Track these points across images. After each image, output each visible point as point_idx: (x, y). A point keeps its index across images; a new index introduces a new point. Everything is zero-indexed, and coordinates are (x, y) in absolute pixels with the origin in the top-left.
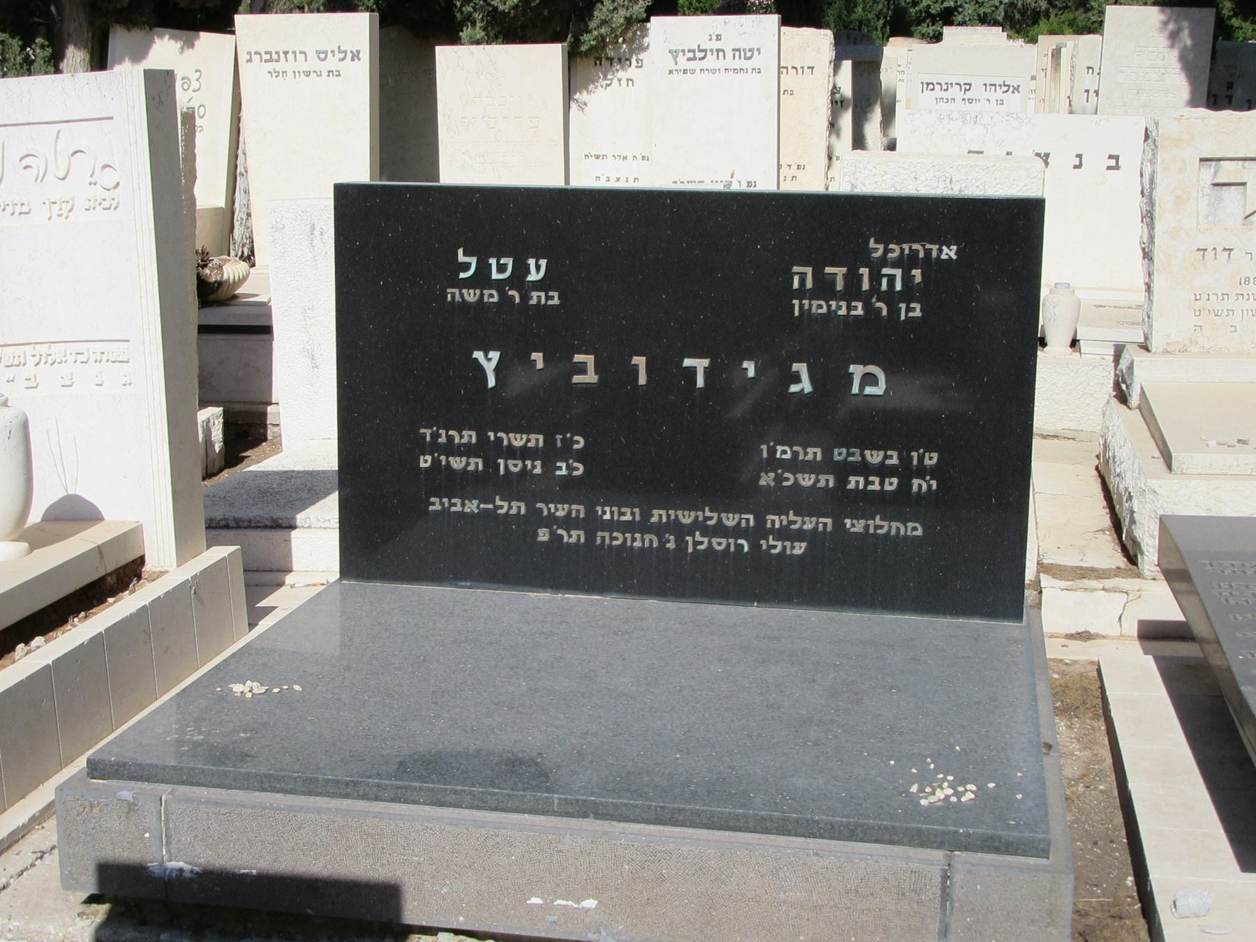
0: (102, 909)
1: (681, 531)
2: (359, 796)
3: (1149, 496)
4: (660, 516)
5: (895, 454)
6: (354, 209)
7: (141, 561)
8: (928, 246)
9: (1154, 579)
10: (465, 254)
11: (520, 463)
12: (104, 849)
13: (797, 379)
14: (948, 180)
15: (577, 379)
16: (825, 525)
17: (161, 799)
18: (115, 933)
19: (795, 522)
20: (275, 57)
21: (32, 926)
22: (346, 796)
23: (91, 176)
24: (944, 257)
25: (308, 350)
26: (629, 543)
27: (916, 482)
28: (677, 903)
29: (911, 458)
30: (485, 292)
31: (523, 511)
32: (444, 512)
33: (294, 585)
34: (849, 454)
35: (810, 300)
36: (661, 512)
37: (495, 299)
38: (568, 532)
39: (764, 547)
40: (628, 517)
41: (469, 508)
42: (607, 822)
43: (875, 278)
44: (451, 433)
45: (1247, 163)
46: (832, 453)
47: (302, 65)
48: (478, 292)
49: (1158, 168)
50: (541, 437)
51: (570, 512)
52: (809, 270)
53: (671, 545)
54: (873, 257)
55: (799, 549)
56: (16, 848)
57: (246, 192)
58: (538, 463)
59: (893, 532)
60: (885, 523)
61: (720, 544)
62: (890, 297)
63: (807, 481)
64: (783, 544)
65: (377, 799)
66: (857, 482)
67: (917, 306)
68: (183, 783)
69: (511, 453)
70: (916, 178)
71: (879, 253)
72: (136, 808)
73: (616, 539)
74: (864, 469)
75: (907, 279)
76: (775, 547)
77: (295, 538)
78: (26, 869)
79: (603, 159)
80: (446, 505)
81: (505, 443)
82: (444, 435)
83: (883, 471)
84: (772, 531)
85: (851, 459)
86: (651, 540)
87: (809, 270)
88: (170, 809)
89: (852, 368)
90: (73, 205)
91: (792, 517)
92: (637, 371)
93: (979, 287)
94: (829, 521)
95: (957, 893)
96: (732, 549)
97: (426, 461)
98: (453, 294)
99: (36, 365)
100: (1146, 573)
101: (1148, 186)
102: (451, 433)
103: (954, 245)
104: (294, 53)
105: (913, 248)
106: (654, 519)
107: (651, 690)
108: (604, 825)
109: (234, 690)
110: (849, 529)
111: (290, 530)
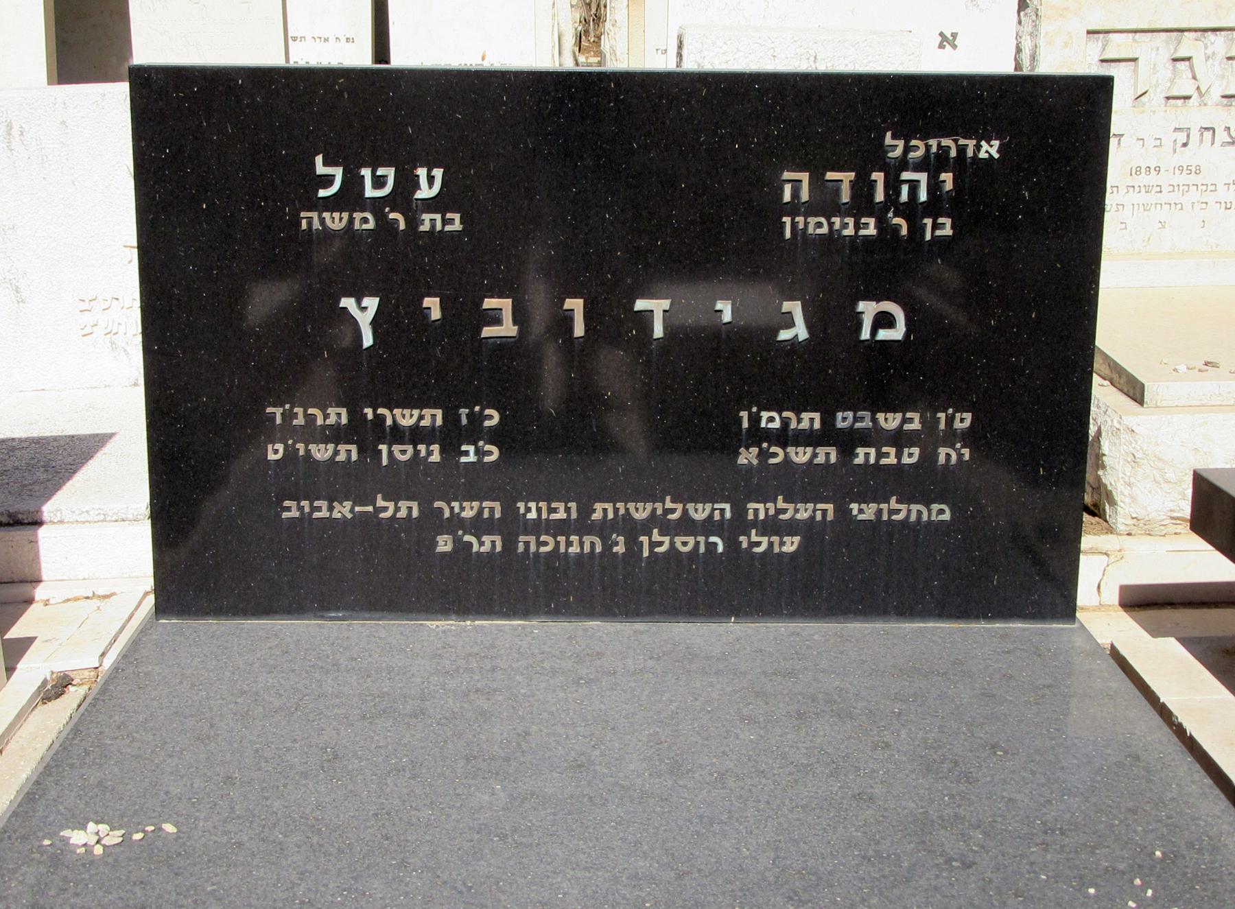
1: (632, 529)
3: (1125, 436)
4: (605, 510)
5: (916, 416)
6: (161, 103)
8: (962, 142)
9: (1129, 534)
10: (325, 164)
11: (410, 449)
14: (812, 58)
15: (487, 332)
16: (824, 512)
19: (785, 511)
25: (10, 280)
26: (562, 549)
27: (942, 451)
30: (355, 215)
31: (415, 513)
32: (304, 519)
33: (48, 600)
34: (856, 419)
35: (806, 216)
36: (606, 505)
37: (371, 225)
38: (479, 538)
39: (745, 545)
40: (561, 515)
41: (340, 512)
43: (893, 185)
44: (310, 411)
46: (834, 419)
48: (345, 215)
49: (1042, 42)
50: (439, 413)
51: (481, 511)
52: (804, 177)
53: (620, 549)
54: (889, 158)
55: (791, 545)
58: (436, 448)
59: (913, 517)
62: (912, 211)
63: (801, 455)
64: (769, 539)
66: (867, 455)
67: (947, 221)
69: (397, 435)
70: (774, 56)
71: (898, 152)
73: (546, 544)
75: (934, 186)
76: (758, 544)
77: (43, 538)
79: (301, 41)
80: (307, 510)
81: (389, 422)
82: (301, 415)
83: (899, 439)
84: (755, 523)
85: (858, 425)
86: (592, 543)
87: (804, 177)
89: (862, 306)
91: (781, 504)
92: (572, 319)
93: (1027, 195)
94: (830, 507)
96: (702, 549)
98: (310, 220)
100: (1121, 527)
101: (1028, 64)
102: (310, 411)
103: (996, 139)
105: (943, 144)
106: (597, 516)
107: (681, 783)
109: (72, 841)
110: (856, 516)
111: (37, 526)
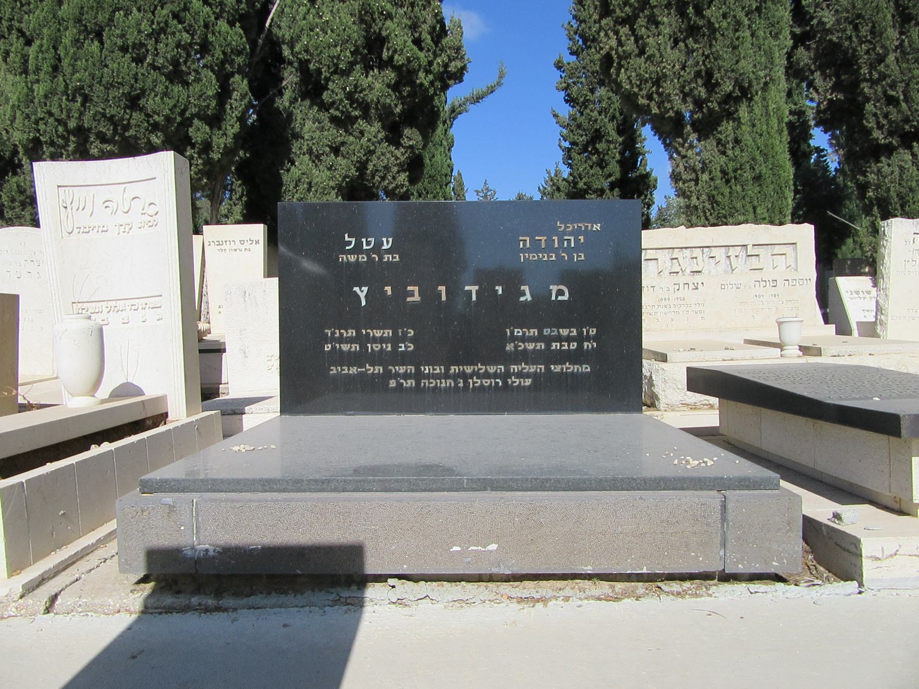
0: (149, 587)
1: (465, 377)
2: (331, 489)
4: (455, 369)
7: (167, 414)
12: (151, 540)
13: (524, 294)
17: (193, 501)
18: (158, 600)
20: (221, 243)
21: (97, 601)
22: (323, 490)
23: (143, 210)
24: (594, 229)
26: (439, 385)
27: (586, 344)
28: (551, 540)
29: (583, 332)
34: (551, 331)
36: (455, 367)
37: (365, 259)
39: (510, 382)
40: (438, 371)
42: (500, 492)
44: (342, 331)
45: (657, 251)
46: (543, 331)
47: (233, 246)
48: (356, 256)
53: (461, 385)
55: (528, 382)
56: (87, 558)
57: (207, 303)
58: (389, 345)
60: (572, 367)
61: (487, 382)
62: (569, 250)
63: (531, 346)
65: (344, 490)
66: (556, 346)
68: (208, 491)
69: (374, 340)
72: (175, 509)
73: (432, 383)
74: (559, 339)
75: (577, 241)
76: (515, 382)
78: (93, 569)
80: (339, 370)
81: (371, 334)
82: (338, 333)
83: (569, 339)
84: (514, 374)
85: (552, 334)
86: (450, 383)
88: (199, 507)
89: (551, 287)
90: (132, 226)
95: (730, 515)
96: (493, 384)
97: (328, 347)
98: (343, 258)
99: (108, 312)
100: (662, 408)
102: (342, 331)
104: (230, 241)
106: (452, 371)
108: (499, 494)
